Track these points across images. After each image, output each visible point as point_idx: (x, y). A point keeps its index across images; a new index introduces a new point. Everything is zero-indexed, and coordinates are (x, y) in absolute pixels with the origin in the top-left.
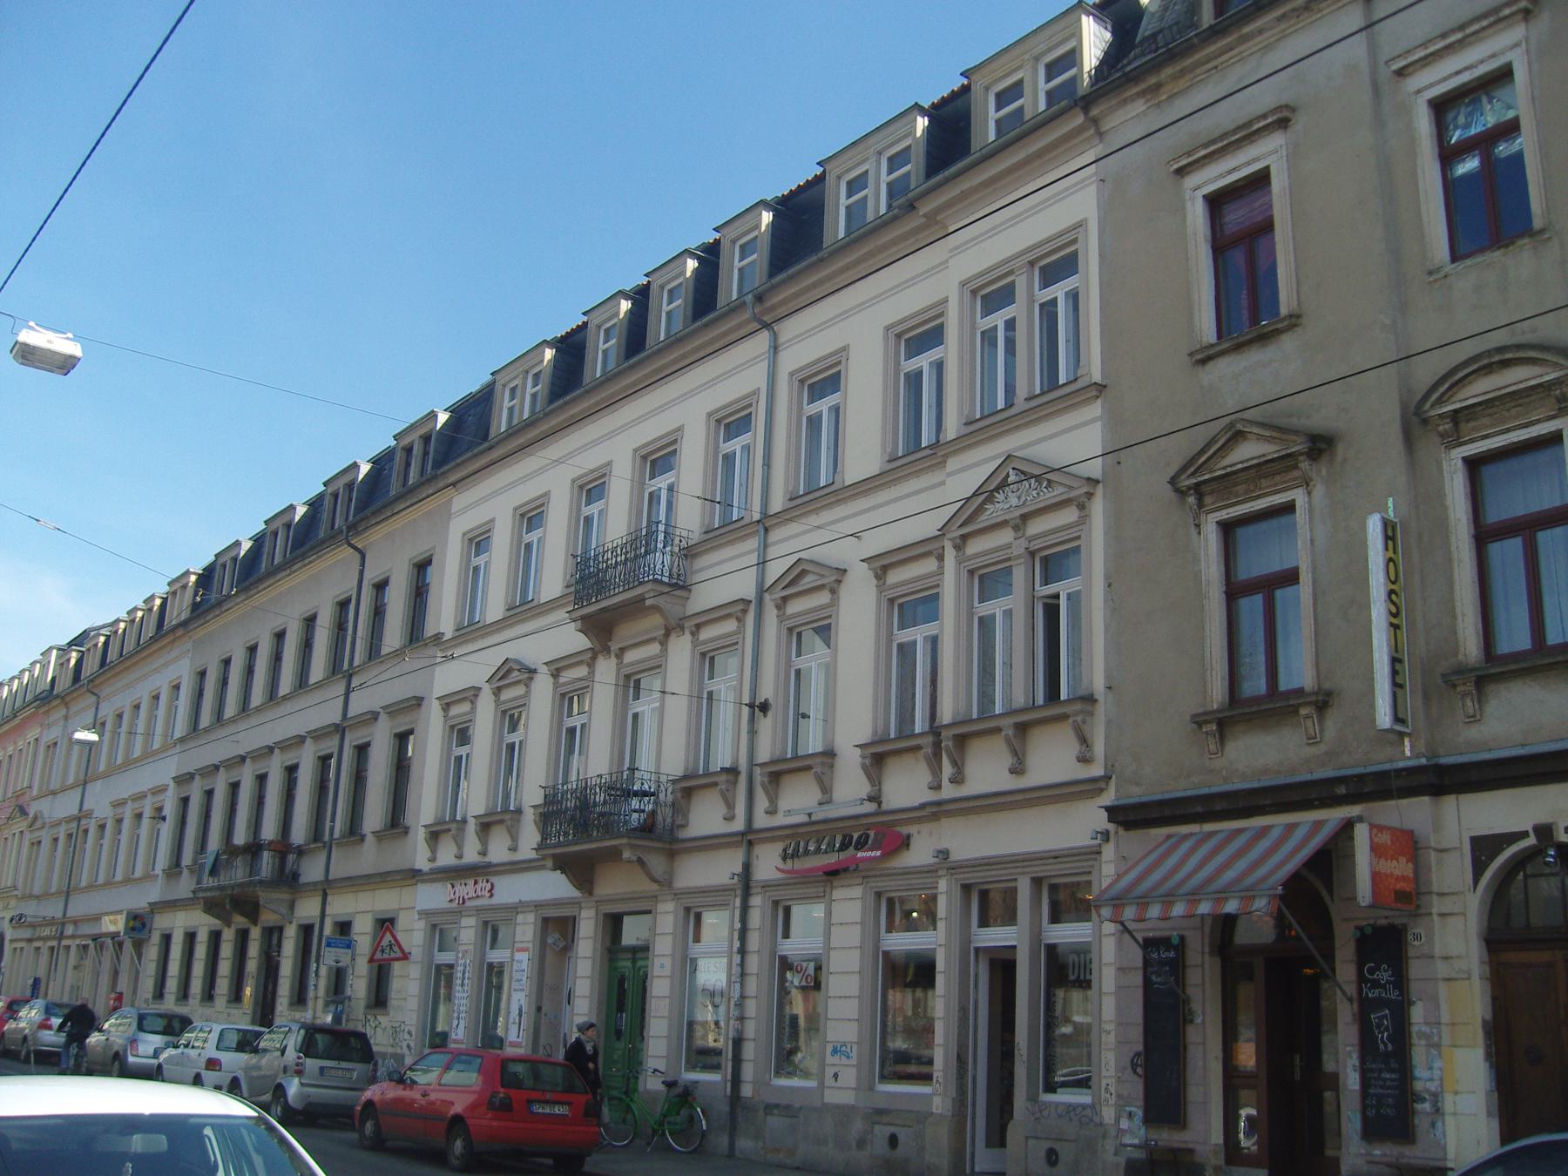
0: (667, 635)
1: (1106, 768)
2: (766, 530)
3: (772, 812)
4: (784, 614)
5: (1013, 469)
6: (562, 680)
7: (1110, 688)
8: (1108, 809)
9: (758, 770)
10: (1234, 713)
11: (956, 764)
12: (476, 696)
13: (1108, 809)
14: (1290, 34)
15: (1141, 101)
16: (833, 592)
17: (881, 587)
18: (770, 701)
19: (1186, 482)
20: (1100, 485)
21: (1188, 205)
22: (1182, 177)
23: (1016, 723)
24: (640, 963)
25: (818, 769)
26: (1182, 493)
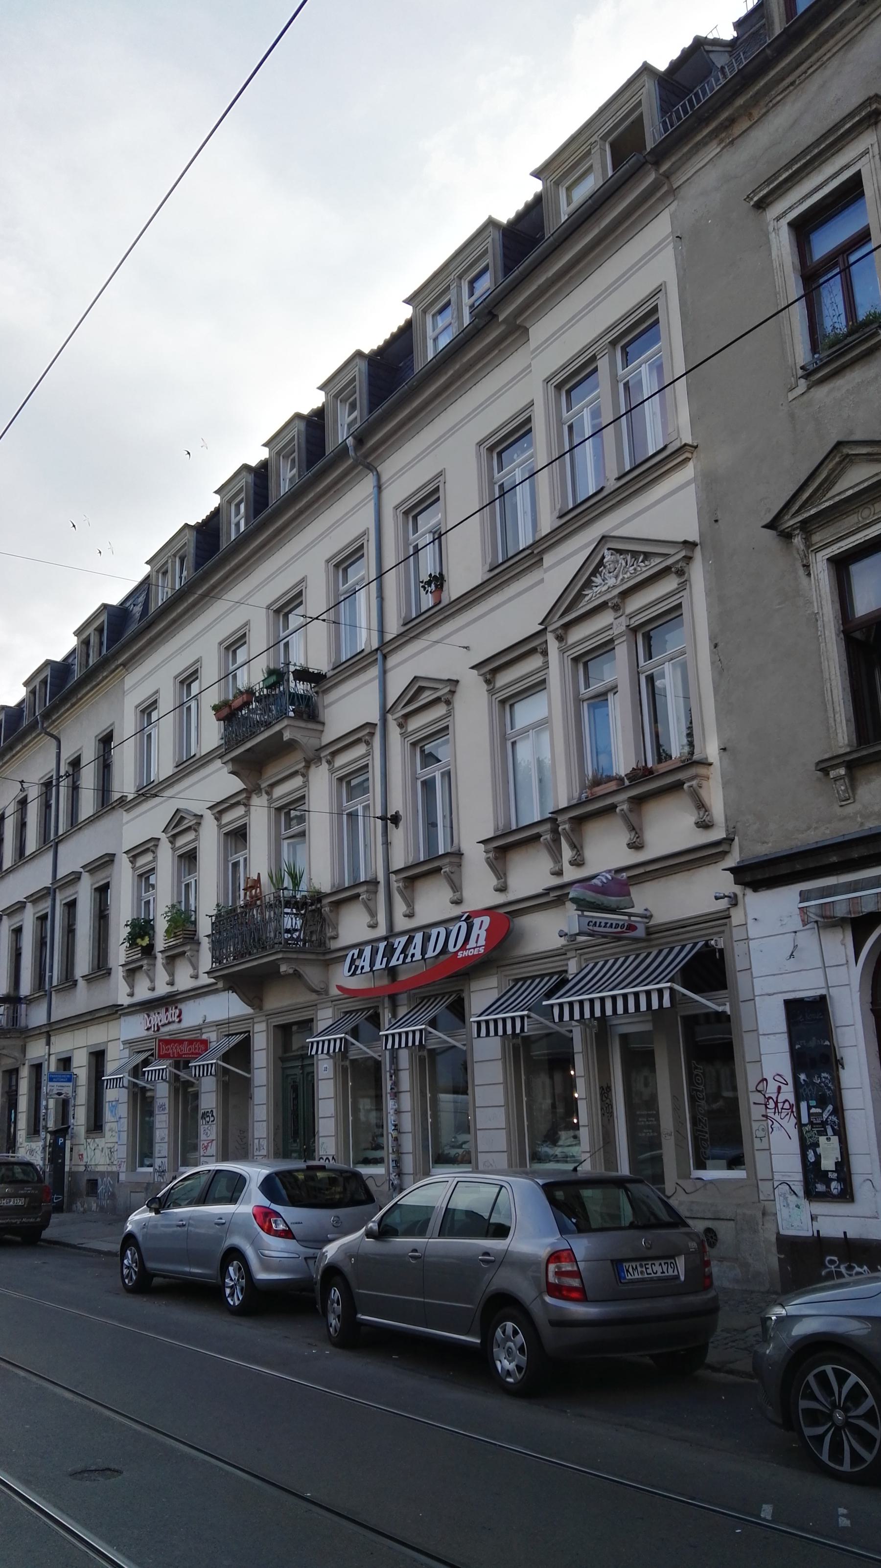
0: (307, 767)
1: (727, 830)
2: (385, 657)
3: (410, 915)
4: (272, 798)
5: (609, 549)
6: (138, 864)
7: (724, 749)
8: (731, 870)
9: (393, 877)
10: (864, 753)
11: (575, 847)
12: (156, 846)
13: (731, 870)
14: (875, 18)
15: (714, 144)
16: (448, 703)
17: (492, 692)
18: (401, 813)
19: (790, 522)
20: (699, 547)
21: (773, 236)
22: (764, 209)
23: (629, 798)
24: (308, 1069)
25: (446, 869)
26: (786, 536)
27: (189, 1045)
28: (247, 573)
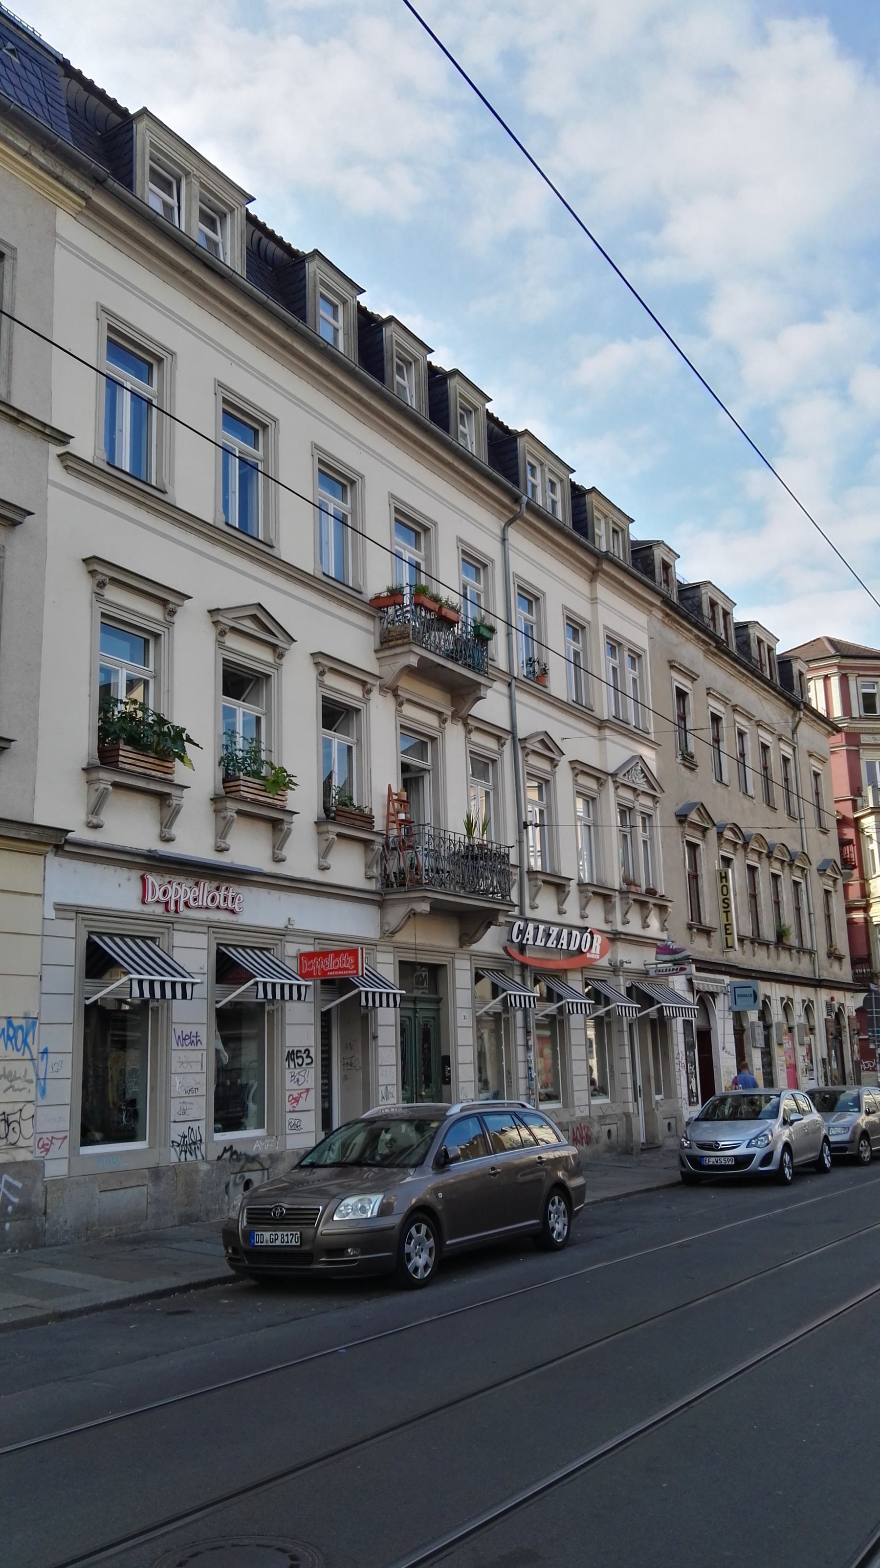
27: (334, 958)
28: (365, 420)
